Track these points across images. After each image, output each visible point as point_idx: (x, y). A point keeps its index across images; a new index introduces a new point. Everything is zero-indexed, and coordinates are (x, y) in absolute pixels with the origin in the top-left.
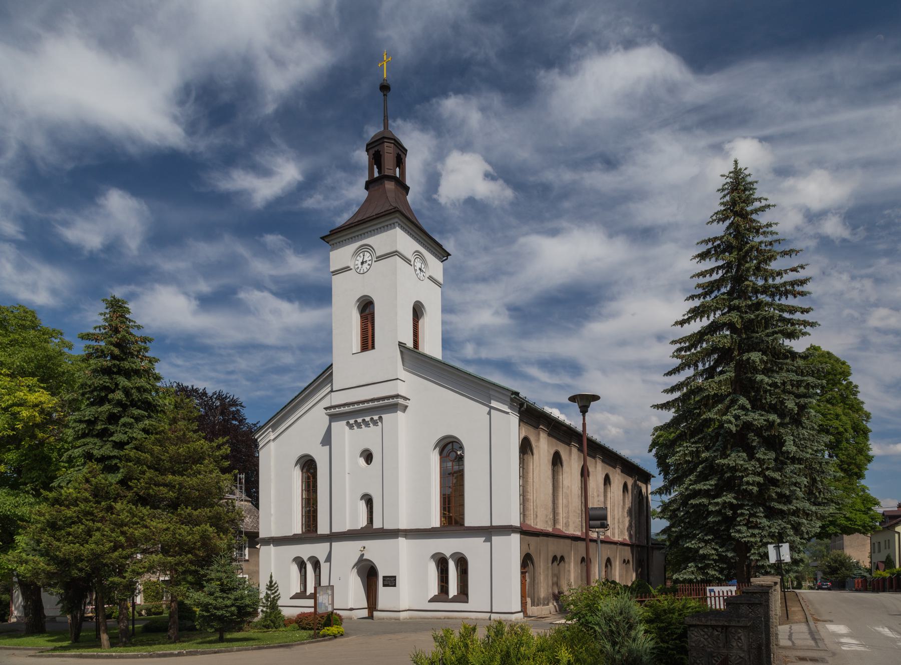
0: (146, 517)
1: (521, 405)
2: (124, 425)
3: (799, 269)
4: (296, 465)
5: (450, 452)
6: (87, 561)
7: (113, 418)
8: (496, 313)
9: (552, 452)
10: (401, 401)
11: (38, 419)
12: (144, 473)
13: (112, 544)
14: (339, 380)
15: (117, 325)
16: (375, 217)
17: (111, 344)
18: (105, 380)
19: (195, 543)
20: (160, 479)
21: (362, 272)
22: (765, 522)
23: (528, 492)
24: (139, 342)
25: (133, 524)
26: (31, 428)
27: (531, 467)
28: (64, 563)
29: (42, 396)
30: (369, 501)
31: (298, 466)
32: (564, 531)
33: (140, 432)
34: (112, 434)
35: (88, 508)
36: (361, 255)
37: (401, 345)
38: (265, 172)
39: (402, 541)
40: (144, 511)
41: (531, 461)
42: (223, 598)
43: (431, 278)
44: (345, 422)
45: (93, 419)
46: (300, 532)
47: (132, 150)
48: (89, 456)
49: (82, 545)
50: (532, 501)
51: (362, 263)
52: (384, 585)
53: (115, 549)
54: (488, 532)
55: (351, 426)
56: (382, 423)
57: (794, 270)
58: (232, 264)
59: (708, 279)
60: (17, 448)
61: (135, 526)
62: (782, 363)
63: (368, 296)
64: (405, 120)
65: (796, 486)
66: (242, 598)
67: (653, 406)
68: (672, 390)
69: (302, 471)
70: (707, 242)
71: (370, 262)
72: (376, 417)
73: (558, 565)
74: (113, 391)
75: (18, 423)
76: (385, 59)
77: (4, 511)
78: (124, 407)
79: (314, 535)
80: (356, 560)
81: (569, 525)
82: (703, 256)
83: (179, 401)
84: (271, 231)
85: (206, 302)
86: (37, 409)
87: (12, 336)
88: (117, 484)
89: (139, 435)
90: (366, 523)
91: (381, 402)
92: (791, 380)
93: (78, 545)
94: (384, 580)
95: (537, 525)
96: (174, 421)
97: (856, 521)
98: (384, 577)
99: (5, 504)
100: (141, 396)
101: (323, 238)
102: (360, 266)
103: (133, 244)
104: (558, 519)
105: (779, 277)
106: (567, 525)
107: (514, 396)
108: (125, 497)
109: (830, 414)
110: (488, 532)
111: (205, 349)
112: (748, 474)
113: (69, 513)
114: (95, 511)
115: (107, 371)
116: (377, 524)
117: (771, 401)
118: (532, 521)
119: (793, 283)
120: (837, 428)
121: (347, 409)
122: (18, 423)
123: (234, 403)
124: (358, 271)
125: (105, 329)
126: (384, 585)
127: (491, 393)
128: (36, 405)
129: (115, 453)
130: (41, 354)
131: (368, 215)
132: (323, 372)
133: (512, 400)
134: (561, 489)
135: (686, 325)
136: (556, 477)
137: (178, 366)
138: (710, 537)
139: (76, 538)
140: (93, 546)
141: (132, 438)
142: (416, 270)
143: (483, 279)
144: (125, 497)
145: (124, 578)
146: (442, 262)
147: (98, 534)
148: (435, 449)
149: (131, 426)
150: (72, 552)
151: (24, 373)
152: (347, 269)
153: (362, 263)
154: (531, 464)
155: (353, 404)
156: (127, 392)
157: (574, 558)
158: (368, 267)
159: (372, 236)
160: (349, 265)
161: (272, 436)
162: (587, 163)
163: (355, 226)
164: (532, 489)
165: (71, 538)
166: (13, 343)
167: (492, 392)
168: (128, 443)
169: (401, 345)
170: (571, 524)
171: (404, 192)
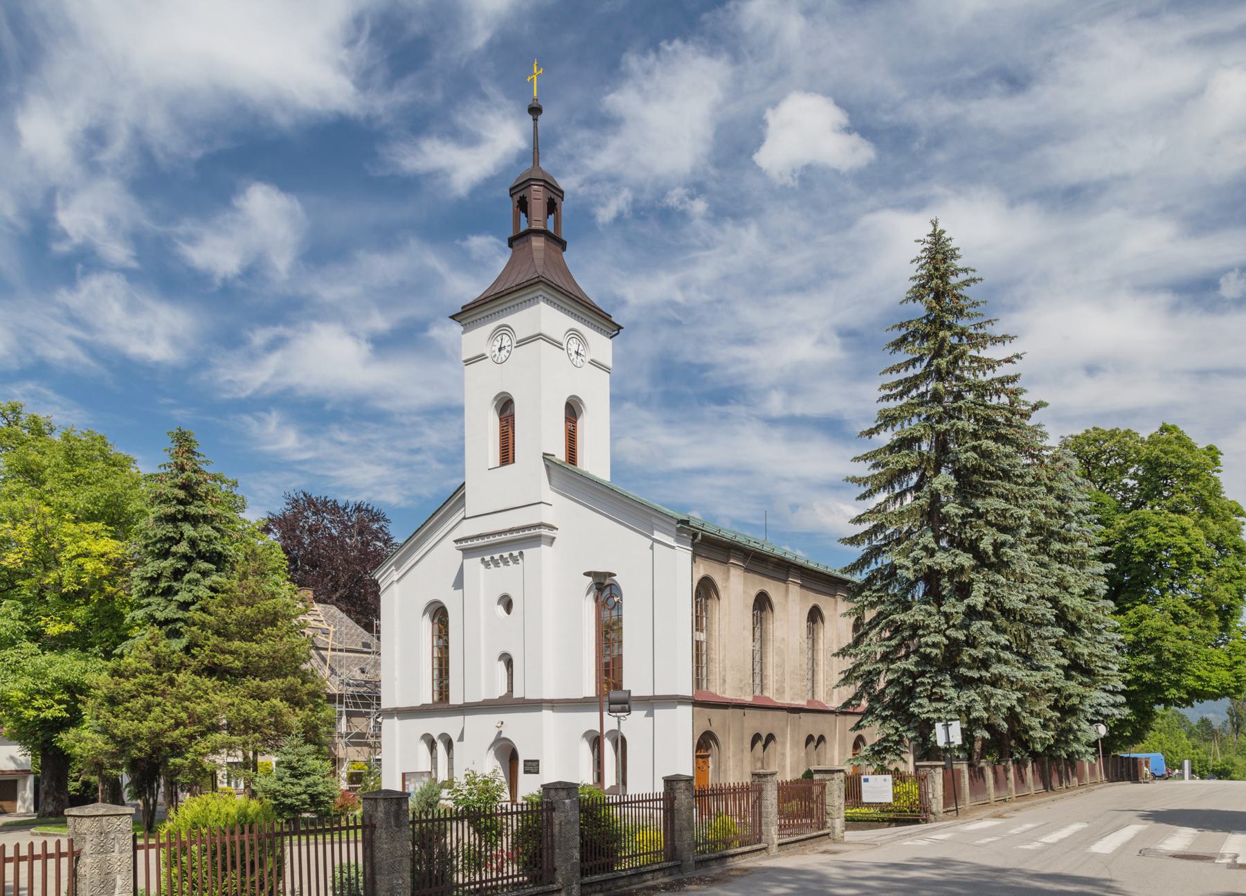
0: (210, 690)
1: (695, 535)
2: (189, 582)
3: (1015, 360)
4: (424, 614)
5: (608, 599)
6: (147, 741)
7: (178, 574)
8: (821, 341)
9: (753, 593)
10: (544, 532)
11: (105, 572)
12: (207, 639)
13: (173, 721)
14: (472, 506)
15: (182, 462)
16: (515, 289)
17: (176, 486)
18: (169, 530)
19: (263, 720)
20: (226, 645)
21: (499, 361)
22: (952, 693)
23: (712, 649)
24: (209, 481)
25: (196, 698)
26: (97, 583)
27: (717, 616)
28: (124, 743)
29: (108, 545)
30: (508, 661)
31: (427, 615)
32: (775, 700)
33: (206, 590)
34: (176, 593)
35: (147, 681)
36: (499, 338)
37: (546, 457)
38: (470, 140)
39: (547, 715)
40: (210, 684)
41: (717, 607)
42: (293, 784)
43: (593, 362)
44: (480, 558)
45: (156, 576)
46: (430, 702)
47: (283, 120)
48: (152, 619)
49: (141, 722)
50: (717, 661)
51: (500, 349)
52: (526, 772)
53: (177, 725)
54: (652, 703)
55: (487, 565)
56: (523, 559)
57: (1008, 361)
58: (420, 285)
59: (903, 375)
60: (86, 603)
61: (198, 700)
62: (991, 485)
63: (503, 393)
64: (685, 40)
65: (992, 647)
66: (316, 784)
67: (840, 540)
68: (859, 520)
69: (433, 621)
70: (901, 326)
71: (509, 348)
72: (516, 553)
73: (816, 747)
74: (178, 542)
75: (84, 575)
76: (535, 71)
77: (71, 678)
78: (190, 560)
79: (445, 706)
80: (492, 739)
81: (784, 692)
82: (899, 344)
83: (250, 553)
84: (478, 230)
85: (383, 345)
86: (103, 560)
87: (78, 471)
88: (181, 651)
89: (204, 593)
90: (506, 691)
91: (521, 533)
92: (995, 509)
93: (136, 721)
94: (525, 765)
95: (725, 693)
96: (244, 576)
97: (1210, 681)
98: (525, 761)
99: (72, 670)
100: (208, 546)
101: (453, 317)
102: (497, 353)
103: (282, 263)
104: (766, 684)
105: (991, 370)
106: (781, 691)
107: (679, 525)
108: (190, 666)
109: (1173, 527)
110: (652, 703)
111: (380, 418)
112: (931, 633)
113: (128, 685)
114: (156, 683)
115: (171, 519)
116: (517, 694)
117: (972, 536)
118: (718, 688)
119: (1001, 381)
120: (1181, 548)
121: (480, 542)
122: (84, 575)
123: (376, 517)
124: (495, 359)
125: (170, 467)
126: (526, 772)
127: (653, 521)
128: (103, 556)
129: (180, 614)
130: (107, 492)
131: (507, 286)
132: (455, 493)
133: (679, 530)
134: (771, 642)
135: (875, 436)
136: (764, 627)
137: (341, 444)
138: (888, 713)
139: (134, 714)
140: (152, 724)
141: (198, 598)
142: (569, 355)
143: (799, 287)
144: (190, 666)
145: (187, 759)
146: (611, 338)
147: (157, 710)
148: (588, 594)
149: (197, 582)
150: (130, 730)
151: (91, 517)
152: (481, 357)
153: (500, 349)
154: (717, 612)
155: (488, 535)
156: (193, 543)
157: (792, 737)
158: (507, 355)
159: (511, 313)
160: (484, 352)
161: (396, 576)
162: (974, 87)
163: (490, 301)
164: (717, 645)
165: (129, 714)
166: (78, 480)
167: (654, 520)
168: (193, 603)
169: (546, 457)
170: (787, 689)
171: (559, 249)
